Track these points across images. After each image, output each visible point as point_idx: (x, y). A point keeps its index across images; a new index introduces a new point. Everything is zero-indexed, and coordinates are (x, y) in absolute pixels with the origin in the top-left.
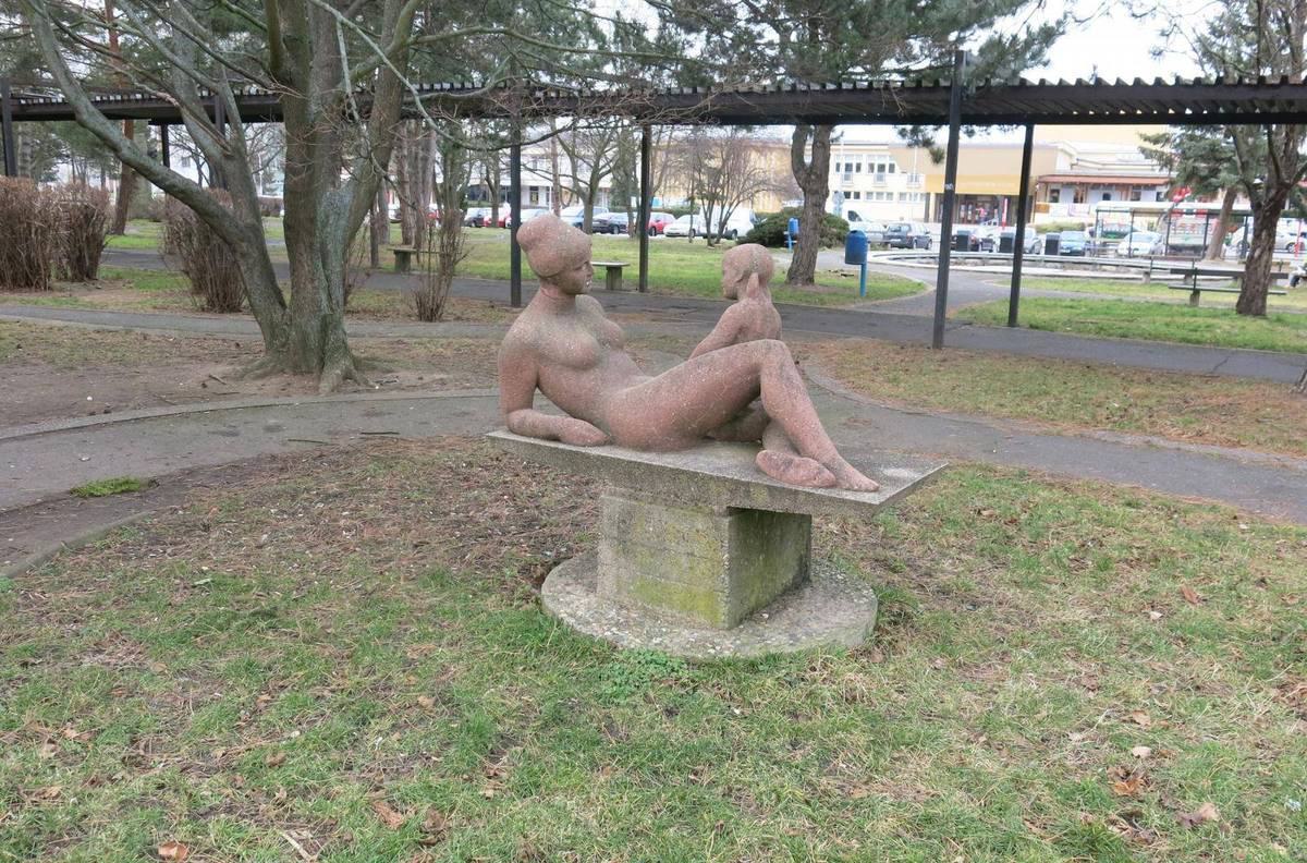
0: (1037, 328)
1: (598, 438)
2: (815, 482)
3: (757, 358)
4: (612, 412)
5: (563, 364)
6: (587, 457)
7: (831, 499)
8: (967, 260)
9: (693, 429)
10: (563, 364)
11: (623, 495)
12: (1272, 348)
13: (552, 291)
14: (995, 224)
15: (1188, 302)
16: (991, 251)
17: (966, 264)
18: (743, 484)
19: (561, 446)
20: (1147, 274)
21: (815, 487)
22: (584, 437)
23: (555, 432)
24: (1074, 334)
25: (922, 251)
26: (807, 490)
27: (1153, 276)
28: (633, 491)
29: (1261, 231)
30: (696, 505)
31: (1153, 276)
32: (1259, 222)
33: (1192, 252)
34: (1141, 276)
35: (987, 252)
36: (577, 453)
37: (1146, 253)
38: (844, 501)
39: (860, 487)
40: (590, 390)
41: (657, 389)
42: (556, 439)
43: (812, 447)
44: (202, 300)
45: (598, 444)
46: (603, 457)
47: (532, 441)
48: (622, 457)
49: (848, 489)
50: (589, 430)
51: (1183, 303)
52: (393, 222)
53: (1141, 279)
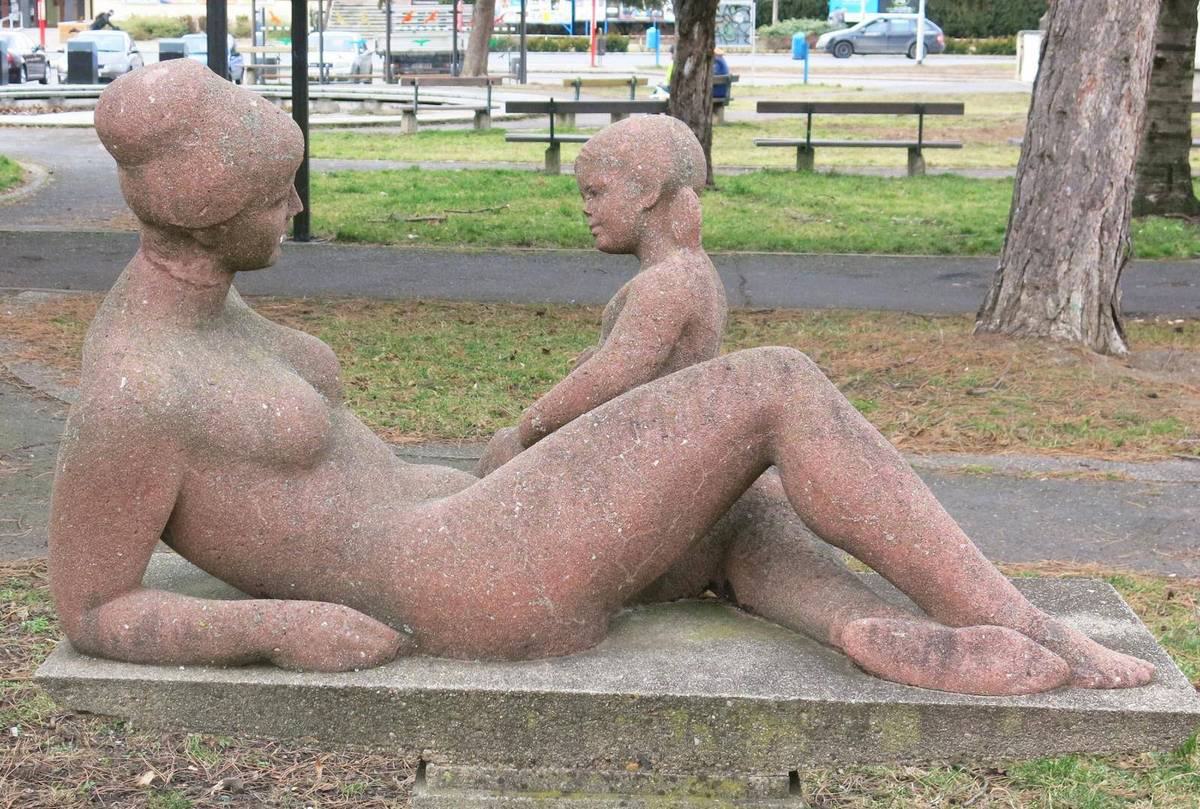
0: (351, 238)
1: (384, 644)
2: (1031, 681)
3: (766, 392)
4: (411, 571)
5: (256, 459)
6: (382, 698)
7: (1090, 717)
8: (20, 103)
9: (627, 587)
10: (256, 459)
11: (480, 783)
12: (787, 245)
13: (195, 265)
14: (16, 24)
15: (543, 166)
16: (43, 81)
17: (18, 111)
18: (852, 710)
19: (295, 680)
20: (410, 113)
21: (1033, 693)
22: (344, 645)
23: (265, 644)
24: (421, 246)
25: (34, 87)
26: (1023, 702)
27: (420, 117)
28: (511, 768)
29: (692, 25)
30: (702, 778)
31: (420, 117)
32: (686, 7)
33: (429, 66)
34: (399, 118)
35: (36, 85)
36: (346, 693)
37: (347, 71)
38: (1124, 717)
39: (1125, 677)
40: (327, 520)
41: (540, 498)
42: (263, 660)
43: (979, 598)
44: (771, 511)
45: (385, 660)
46: (429, 694)
47: (181, 675)
48: (465, 687)
49: (1101, 687)
50: (360, 626)
51: (533, 168)
52: (633, 96)
53: (397, 124)
